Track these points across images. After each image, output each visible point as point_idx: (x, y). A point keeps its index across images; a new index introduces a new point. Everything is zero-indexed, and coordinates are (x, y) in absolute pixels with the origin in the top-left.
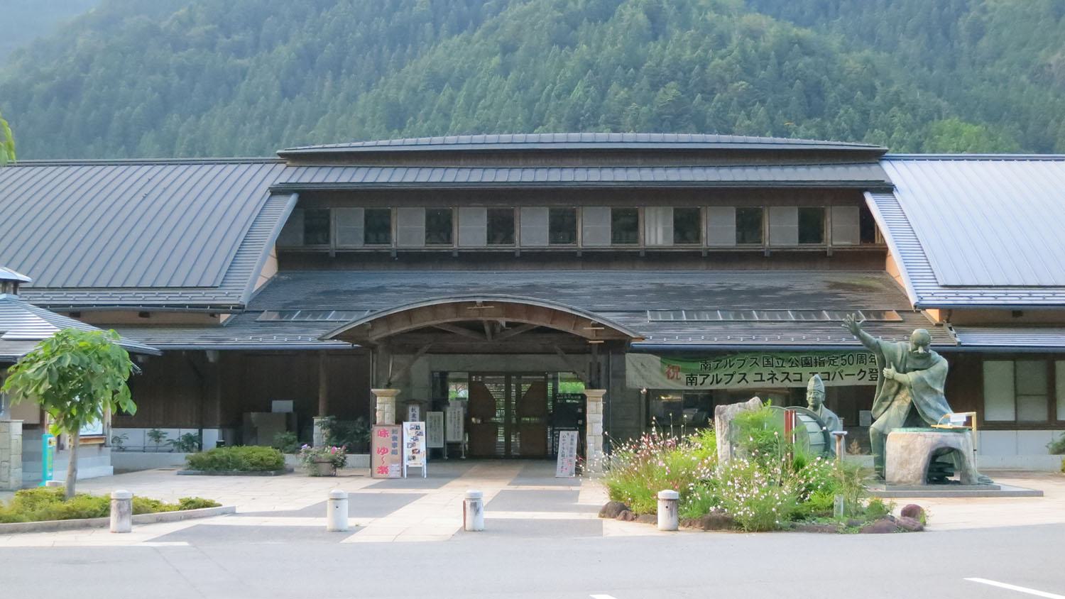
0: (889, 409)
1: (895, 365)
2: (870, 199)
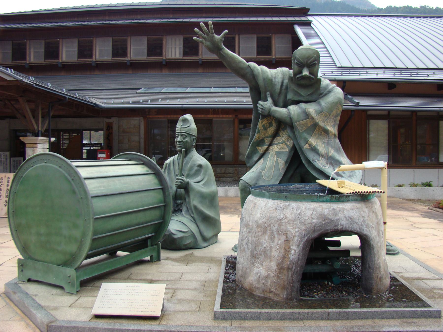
0: (265, 156)
1: (272, 97)
2: (299, 30)
